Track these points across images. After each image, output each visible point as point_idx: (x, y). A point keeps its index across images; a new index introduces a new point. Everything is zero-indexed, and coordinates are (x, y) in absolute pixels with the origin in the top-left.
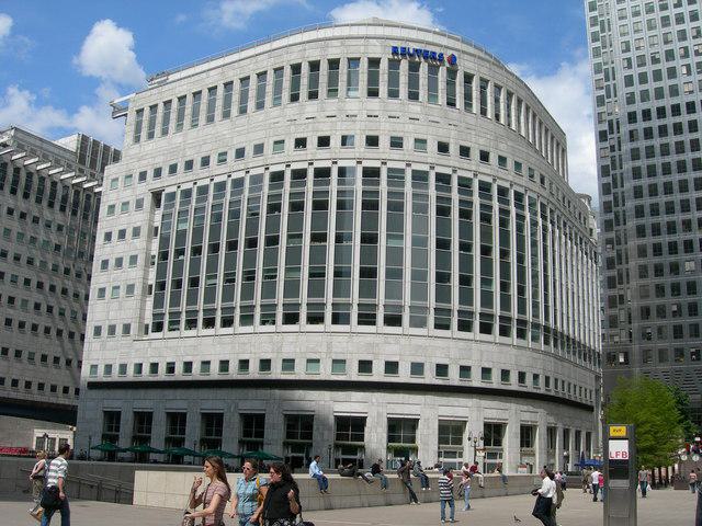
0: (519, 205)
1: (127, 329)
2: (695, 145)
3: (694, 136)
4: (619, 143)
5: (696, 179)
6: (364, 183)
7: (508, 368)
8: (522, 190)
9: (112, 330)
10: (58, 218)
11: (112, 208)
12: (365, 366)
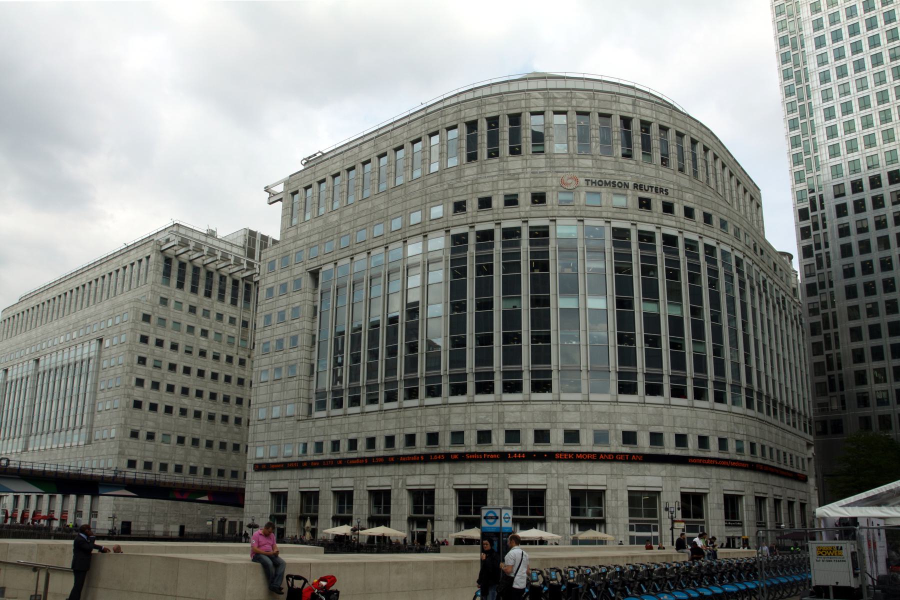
2: (892, 307)
3: (891, 296)
5: (893, 346)
7: (705, 434)
8: (712, 243)
10: (226, 308)
11: (270, 291)
12: (542, 436)
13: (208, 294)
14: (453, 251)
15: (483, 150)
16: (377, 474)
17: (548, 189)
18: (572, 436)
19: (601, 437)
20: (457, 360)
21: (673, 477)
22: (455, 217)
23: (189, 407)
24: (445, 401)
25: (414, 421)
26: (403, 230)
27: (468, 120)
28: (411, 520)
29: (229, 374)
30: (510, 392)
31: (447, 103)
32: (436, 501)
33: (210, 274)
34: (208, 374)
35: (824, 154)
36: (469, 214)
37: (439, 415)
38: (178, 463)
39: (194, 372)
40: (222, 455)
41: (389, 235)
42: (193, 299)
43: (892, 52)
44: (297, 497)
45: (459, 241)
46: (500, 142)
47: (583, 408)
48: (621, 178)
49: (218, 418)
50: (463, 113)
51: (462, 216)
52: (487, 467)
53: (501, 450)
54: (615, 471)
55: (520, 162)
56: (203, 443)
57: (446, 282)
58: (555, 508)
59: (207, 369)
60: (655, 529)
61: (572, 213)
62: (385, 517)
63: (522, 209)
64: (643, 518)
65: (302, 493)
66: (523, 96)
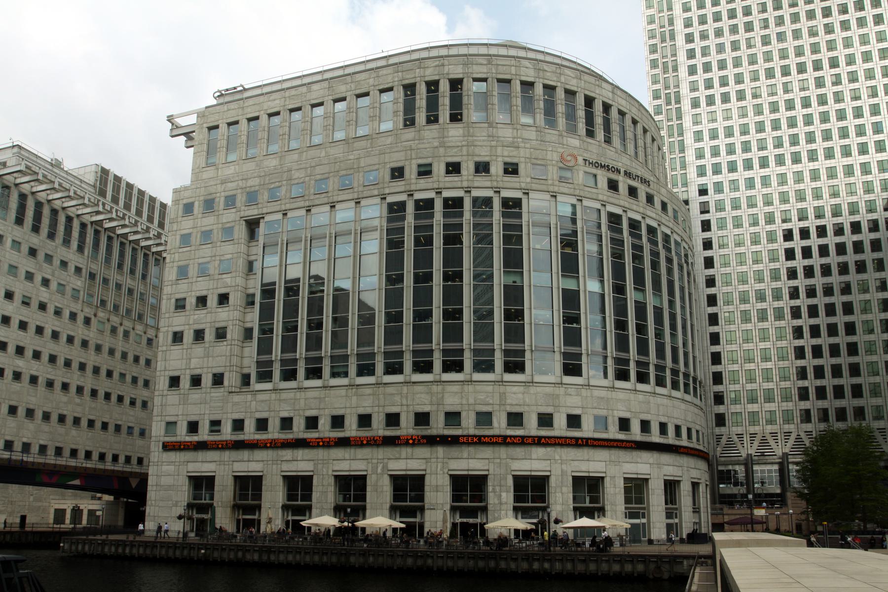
0: (654, 243)
1: (218, 380)
4: (607, 168)
6: (445, 215)
9: (196, 381)
10: (71, 255)
12: (545, 420)
13: (51, 236)
14: (390, 220)
15: (421, 116)
16: (347, 456)
17: (549, 162)
18: (574, 421)
19: (602, 422)
20: (393, 335)
21: (659, 465)
22: (447, 179)
23: (24, 371)
24: (437, 378)
25: (397, 398)
26: (381, 186)
27: (452, 76)
28: (285, 508)
29: (72, 334)
30: (421, 372)
31: (453, 51)
32: (427, 488)
33: (54, 212)
34: (48, 332)
35: (692, 172)
36: (465, 178)
37: (430, 393)
38: (8, 438)
39: (32, 328)
40: (61, 429)
41: (361, 189)
42: (35, 240)
43: (754, 91)
44: (230, 482)
45: (396, 210)
46: (440, 108)
47: (584, 392)
48: (614, 163)
49: (58, 386)
50: (446, 68)
51: (456, 179)
52: (487, 452)
53: (503, 433)
54: (613, 458)
55: (511, 131)
56: (39, 415)
57: (381, 253)
58: (559, 495)
59: (47, 326)
60: (644, 517)
61: (571, 191)
62: (207, 504)
63: (522, 179)
64: (634, 506)
65: (236, 477)
66: (513, 62)
